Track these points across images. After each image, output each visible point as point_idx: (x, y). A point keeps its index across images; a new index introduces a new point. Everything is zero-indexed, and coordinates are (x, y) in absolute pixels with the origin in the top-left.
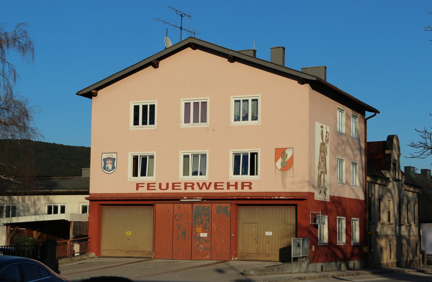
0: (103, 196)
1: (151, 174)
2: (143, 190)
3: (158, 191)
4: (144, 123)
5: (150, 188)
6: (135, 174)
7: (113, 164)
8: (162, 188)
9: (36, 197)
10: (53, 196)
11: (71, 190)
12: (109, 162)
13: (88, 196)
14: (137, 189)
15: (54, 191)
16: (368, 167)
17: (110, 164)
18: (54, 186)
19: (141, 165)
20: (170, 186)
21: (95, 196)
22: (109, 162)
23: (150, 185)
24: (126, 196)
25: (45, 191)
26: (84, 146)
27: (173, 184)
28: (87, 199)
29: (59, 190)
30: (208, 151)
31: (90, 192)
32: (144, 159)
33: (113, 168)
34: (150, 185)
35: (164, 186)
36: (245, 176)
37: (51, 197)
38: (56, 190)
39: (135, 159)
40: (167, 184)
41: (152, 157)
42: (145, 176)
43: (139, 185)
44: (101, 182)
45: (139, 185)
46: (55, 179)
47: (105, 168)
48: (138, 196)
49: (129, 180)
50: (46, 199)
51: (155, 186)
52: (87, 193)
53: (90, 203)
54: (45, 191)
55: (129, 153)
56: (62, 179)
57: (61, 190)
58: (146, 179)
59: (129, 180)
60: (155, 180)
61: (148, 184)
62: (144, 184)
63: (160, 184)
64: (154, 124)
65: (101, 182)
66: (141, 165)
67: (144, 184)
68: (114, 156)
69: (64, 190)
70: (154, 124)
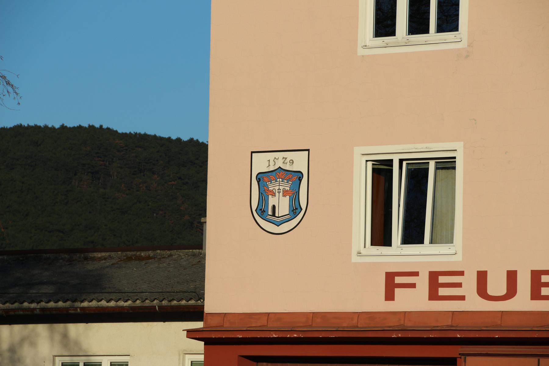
0: (255, 324)
1: (443, 236)
2: (413, 301)
3: (474, 303)
4: (418, 25)
5: (442, 292)
6: (381, 236)
7: (295, 196)
8: (491, 291)
9: (17, 328)
10: (81, 326)
11: (147, 303)
12: (278, 186)
13: (199, 325)
14: (390, 296)
15: (85, 304)
16: (202, 230)
17: (281, 192)
18: (95, 285)
19: (405, 200)
20: (524, 284)
21: (227, 326)
22: (278, 186)
23: (442, 279)
24: (345, 324)
25: (52, 304)
26: (111, 127)
27: (536, 275)
28: (191, 334)
29: (104, 303)
30: (459, 146)
31: (208, 309)
32: (417, 176)
33: (295, 210)
34: (442, 279)
35: (497, 285)
36: (413, 249)
37: (75, 330)
38: (94, 304)
39: (382, 172)
40: (512, 276)
41: (447, 165)
42: (421, 241)
43: (398, 280)
44: (249, 271)
45: (398, 280)
46: (100, 259)
47: (262, 211)
48: (393, 323)
49: (355, 259)
50: (57, 337)
51: (459, 285)
52: (197, 314)
53: (206, 354)
54: (52, 304)
55: (358, 150)
56: (129, 259)
57: (112, 304)
58: (424, 256)
59: (355, 259)
60: (459, 258)
61: (434, 276)
62: (416, 274)
63: (482, 277)
64: (456, 29)
65: (249, 271)
66: (405, 200)
67: (416, 274)
68: (299, 162)
69: (121, 303)
70: (456, 29)
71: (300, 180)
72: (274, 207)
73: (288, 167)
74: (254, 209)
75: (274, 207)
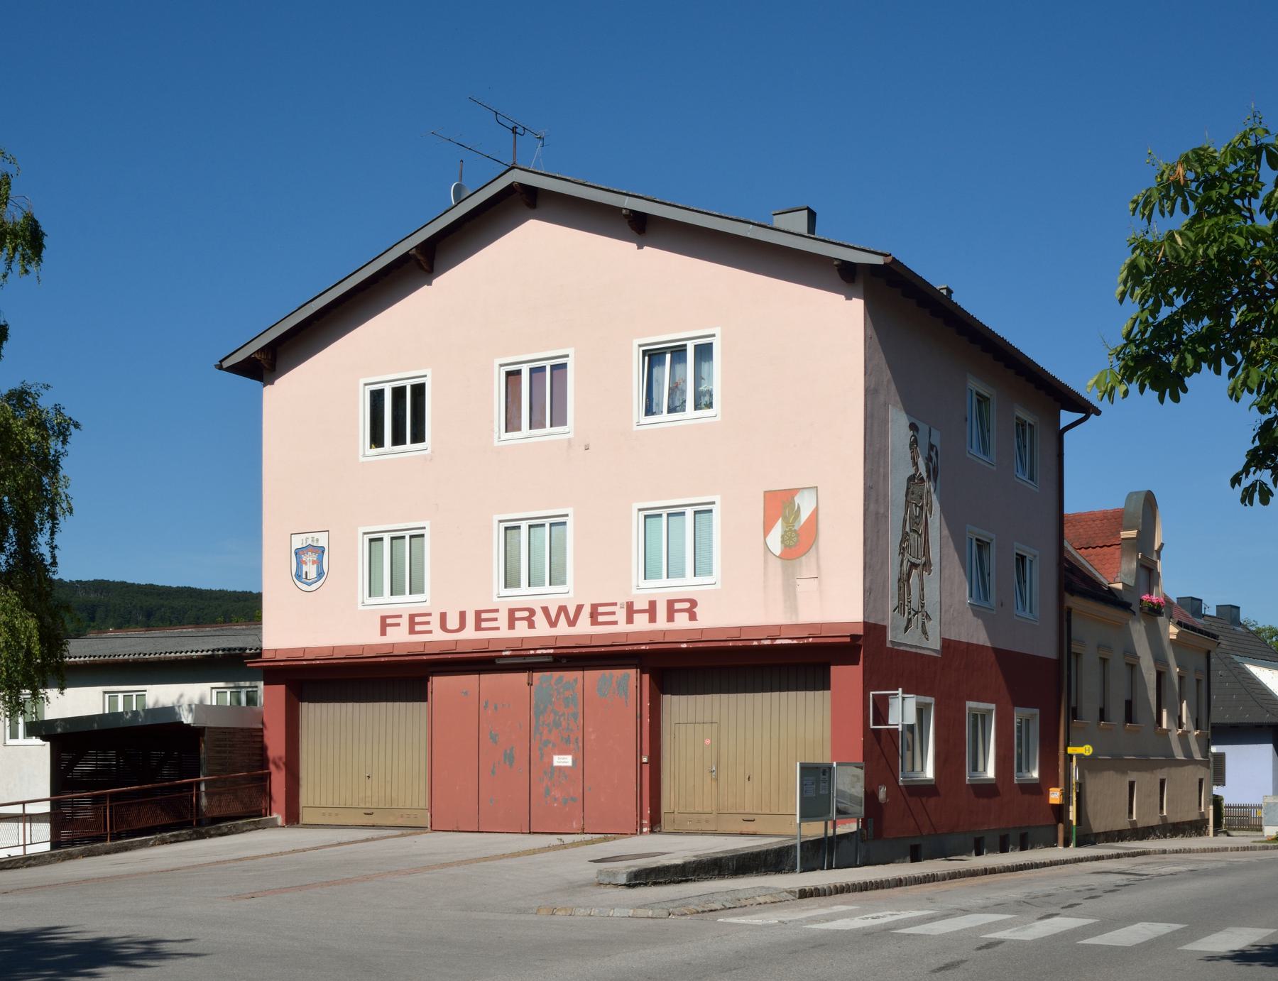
33: (320, 574)
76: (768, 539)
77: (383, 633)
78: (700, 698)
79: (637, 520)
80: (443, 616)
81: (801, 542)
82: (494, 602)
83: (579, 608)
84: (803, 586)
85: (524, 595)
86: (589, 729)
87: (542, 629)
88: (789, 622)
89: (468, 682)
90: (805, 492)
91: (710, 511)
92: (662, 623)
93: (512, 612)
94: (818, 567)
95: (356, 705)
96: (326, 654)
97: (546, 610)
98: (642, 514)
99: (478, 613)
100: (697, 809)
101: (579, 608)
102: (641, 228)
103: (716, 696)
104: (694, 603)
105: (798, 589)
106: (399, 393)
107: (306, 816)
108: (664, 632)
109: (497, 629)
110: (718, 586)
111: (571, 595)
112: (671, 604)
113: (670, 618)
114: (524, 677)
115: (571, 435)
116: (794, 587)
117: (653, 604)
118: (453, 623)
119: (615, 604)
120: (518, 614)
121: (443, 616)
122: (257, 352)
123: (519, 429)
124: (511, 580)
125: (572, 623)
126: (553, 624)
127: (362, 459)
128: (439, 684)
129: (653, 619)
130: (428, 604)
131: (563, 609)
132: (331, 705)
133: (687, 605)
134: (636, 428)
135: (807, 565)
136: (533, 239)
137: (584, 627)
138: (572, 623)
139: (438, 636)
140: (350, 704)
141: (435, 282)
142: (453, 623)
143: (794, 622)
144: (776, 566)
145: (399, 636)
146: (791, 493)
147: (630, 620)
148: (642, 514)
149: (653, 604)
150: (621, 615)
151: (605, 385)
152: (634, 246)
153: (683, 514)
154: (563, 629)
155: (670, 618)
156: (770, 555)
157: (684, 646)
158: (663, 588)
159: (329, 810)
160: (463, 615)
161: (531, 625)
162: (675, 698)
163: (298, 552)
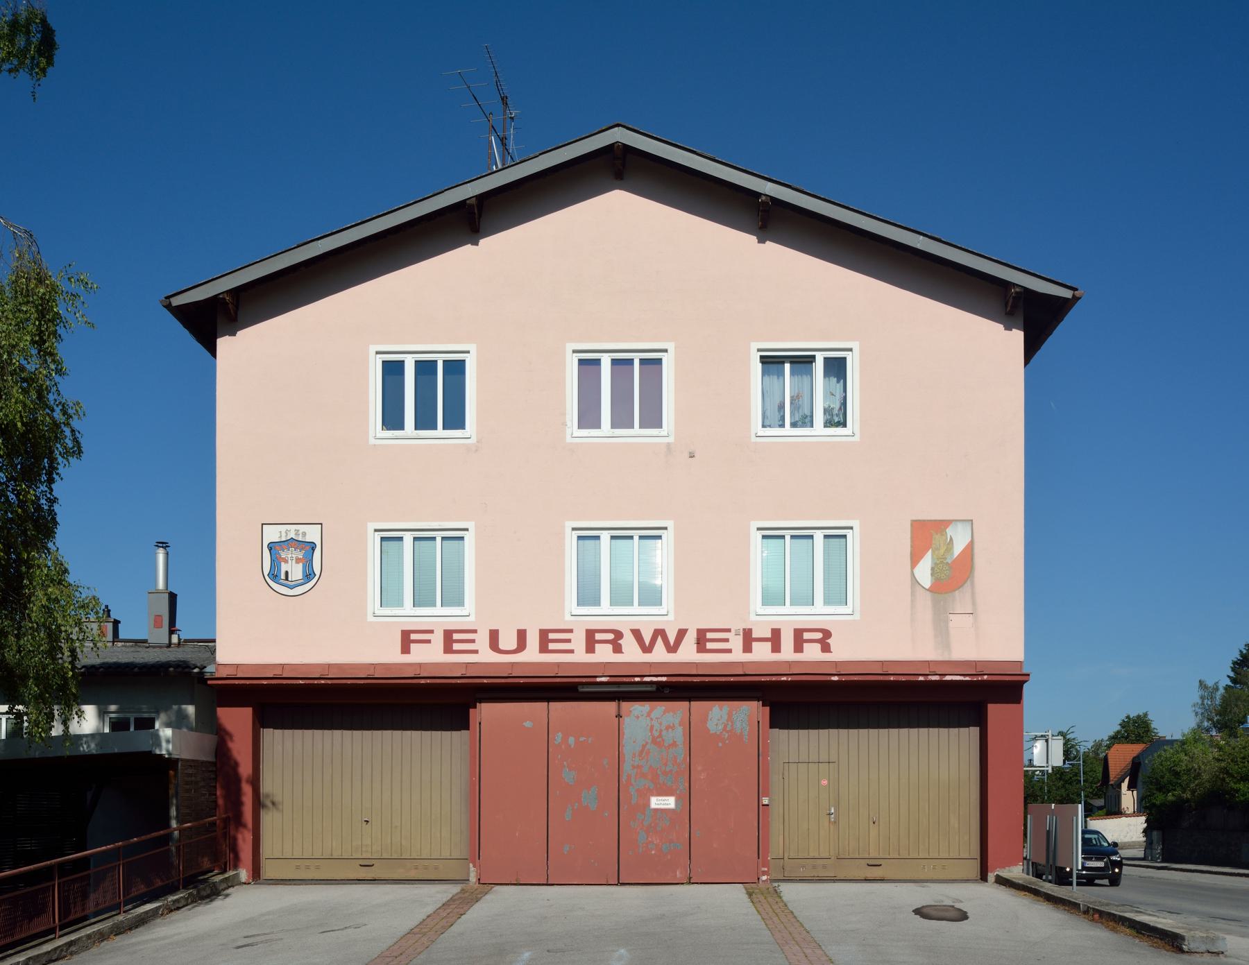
33: (309, 575)
68: (312, 534)
71: (313, 549)
72: (287, 573)
73: (300, 539)
74: (266, 574)
75: (287, 573)
76: (916, 571)
77: (406, 649)
78: (813, 733)
79: (374, 541)
80: (494, 636)
81: (955, 576)
82: (567, 621)
83: (682, 633)
84: (956, 622)
85: (605, 613)
86: (697, 767)
87: (631, 653)
88: (940, 659)
89: (529, 713)
90: (960, 525)
91: (462, 538)
92: (787, 653)
93: (590, 634)
94: (974, 604)
95: (347, 733)
96: (370, 673)
97: (637, 634)
98: (378, 536)
99: (544, 634)
100: (811, 855)
101: (682, 633)
102: (468, 221)
103: (834, 732)
104: (827, 634)
105: (951, 624)
106: (425, 369)
107: (268, 871)
108: (789, 664)
109: (729, 651)
110: (857, 617)
111: (671, 617)
112: (798, 633)
113: (798, 648)
114: (610, 707)
115: (671, 440)
116: (947, 621)
117: (776, 634)
118: (508, 641)
119: (729, 630)
120: (598, 636)
121: (494, 636)
122: (227, 292)
123: (598, 426)
124: (588, 596)
125: (672, 649)
126: (647, 649)
127: (372, 441)
128: (487, 713)
129: (776, 648)
130: (472, 618)
131: (660, 633)
132: (308, 733)
133: (611, 636)
134: (754, 439)
135: (961, 600)
136: (618, 211)
137: (688, 654)
138: (672, 649)
139: (486, 656)
140: (337, 733)
141: (482, 242)
142: (508, 641)
143: (947, 659)
144: (925, 600)
145: (429, 655)
146: (941, 525)
147: (747, 648)
148: (378, 536)
149: (776, 634)
150: (736, 643)
151: (714, 389)
152: (754, 239)
153: (401, 539)
154: (660, 654)
155: (798, 648)
156: (918, 588)
157: (835, 678)
158: (789, 616)
159: (307, 863)
160: (522, 635)
161: (618, 649)
162: (278, 733)
163: (271, 547)
